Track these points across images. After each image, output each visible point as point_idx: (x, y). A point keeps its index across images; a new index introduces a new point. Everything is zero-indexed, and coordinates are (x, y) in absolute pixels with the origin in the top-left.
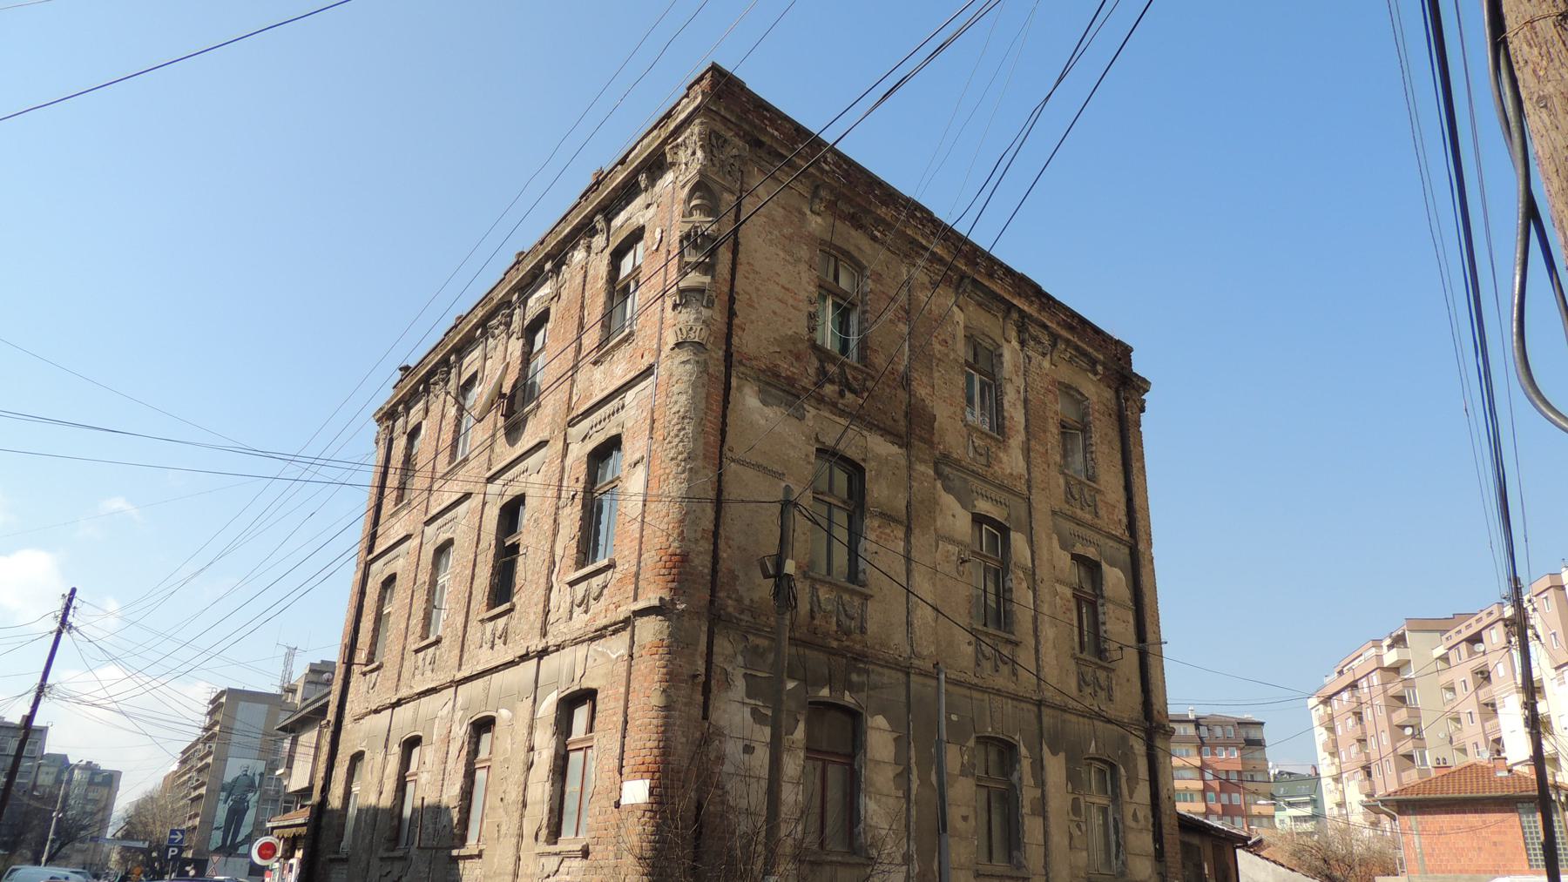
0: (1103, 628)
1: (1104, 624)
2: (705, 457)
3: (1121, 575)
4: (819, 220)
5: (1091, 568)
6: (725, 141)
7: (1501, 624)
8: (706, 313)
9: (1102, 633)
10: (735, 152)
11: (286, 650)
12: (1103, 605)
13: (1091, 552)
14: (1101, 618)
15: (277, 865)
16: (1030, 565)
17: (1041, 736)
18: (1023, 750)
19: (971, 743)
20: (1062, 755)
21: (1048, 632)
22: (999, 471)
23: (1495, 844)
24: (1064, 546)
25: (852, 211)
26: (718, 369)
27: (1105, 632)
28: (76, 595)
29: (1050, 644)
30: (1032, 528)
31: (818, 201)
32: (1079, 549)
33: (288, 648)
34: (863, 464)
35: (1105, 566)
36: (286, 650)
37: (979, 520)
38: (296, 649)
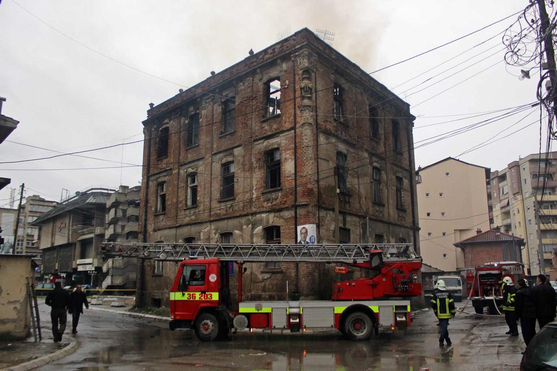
0: (403, 199)
2: (314, 159)
3: (408, 181)
4: (333, 76)
5: (399, 180)
7: (496, 179)
8: (311, 113)
10: (314, 58)
11: (11, 190)
13: (400, 175)
15: (399, 286)
16: (386, 180)
18: (385, 237)
19: (374, 236)
20: (394, 239)
21: (391, 201)
22: (378, 152)
23: (494, 256)
26: (315, 131)
28: (25, 186)
29: (391, 206)
32: (397, 175)
33: (12, 189)
34: (347, 155)
35: (404, 179)
36: (11, 190)
37: (374, 168)
38: (15, 189)
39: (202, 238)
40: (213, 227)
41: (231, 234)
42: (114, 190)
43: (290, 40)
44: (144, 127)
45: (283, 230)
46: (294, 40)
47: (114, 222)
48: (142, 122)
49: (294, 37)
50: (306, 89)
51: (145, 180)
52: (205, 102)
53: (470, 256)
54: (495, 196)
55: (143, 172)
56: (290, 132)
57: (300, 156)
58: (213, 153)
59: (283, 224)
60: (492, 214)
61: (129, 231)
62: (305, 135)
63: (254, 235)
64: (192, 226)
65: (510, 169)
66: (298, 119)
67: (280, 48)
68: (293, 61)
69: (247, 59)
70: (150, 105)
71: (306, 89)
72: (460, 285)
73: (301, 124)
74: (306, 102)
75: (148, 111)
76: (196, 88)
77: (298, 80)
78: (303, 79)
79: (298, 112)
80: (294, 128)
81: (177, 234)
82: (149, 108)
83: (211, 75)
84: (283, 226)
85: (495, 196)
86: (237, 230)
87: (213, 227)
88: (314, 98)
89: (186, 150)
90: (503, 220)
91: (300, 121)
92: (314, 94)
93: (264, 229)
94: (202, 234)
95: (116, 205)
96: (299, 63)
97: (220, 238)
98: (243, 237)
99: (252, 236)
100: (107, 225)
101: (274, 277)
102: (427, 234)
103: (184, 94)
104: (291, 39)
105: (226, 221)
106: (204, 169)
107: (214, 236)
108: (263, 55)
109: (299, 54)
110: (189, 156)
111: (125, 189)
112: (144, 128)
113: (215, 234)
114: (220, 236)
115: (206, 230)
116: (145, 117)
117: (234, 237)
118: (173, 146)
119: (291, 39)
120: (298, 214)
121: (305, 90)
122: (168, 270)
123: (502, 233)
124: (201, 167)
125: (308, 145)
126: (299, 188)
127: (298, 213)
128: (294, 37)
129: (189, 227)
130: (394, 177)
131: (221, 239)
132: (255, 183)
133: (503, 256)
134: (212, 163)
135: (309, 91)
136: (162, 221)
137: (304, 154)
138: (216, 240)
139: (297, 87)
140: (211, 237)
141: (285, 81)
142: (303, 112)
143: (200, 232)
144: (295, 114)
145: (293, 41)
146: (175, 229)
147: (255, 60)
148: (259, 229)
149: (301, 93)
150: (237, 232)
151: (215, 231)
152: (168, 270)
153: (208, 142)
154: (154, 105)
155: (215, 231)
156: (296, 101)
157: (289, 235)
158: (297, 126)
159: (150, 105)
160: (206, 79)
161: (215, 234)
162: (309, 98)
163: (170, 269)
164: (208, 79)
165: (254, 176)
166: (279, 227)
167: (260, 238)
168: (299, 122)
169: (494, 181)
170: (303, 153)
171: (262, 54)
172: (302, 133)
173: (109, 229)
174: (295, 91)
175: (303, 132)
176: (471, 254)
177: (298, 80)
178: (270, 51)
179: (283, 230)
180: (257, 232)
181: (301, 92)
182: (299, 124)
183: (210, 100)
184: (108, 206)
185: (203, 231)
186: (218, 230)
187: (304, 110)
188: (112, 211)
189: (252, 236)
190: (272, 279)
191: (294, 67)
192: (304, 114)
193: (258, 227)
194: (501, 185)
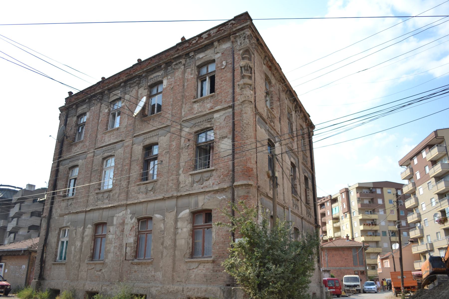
1: (309, 196)
6: (252, 37)
9: (308, 198)
12: (308, 190)
14: (308, 194)
17: (303, 228)
23: (346, 259)
24: (303, 173)
31: (265, 60)
39: (115, 222)
40: (129, 211)
41: (151, 218)
42: (21, 188)
43: (228, 24)
45: (216, 213)
46: (233, 24)
47: (18, 216)
49: (233, 22)
51: (56, 164)
53: (326, 258)
56: (226, 111)
57: (239, 134)
58: (135, 135)
59: (215, 207)
61: (31, 225)
62: (245, 113)
65: (341, 193)
67: (216, 32)
68: (233, 42)
72: (359, 282)
73: (241, 101)
74: (247, 80)
75: (66, 99)
77: (237, 59)
78: (243, 58)
79: (237, 90)
80: (233, 107)
82: (67, 96)
83: (137, 62)
84: (215, 209)
85: (329, 214)
86: (158, 214)
89: (104, 133)
90: (334, 233)
91: (240, 99)
92: (253, 74)
94: (115, 219)
95: (21, 201)
97: (136, 223)
98: (165, 221)
100: (11, 219)
101: (203, 267)
102: (57, 287)
103: (106, 81)
105: (145, 205)
106: (123, 152)
107: (130, 220)
108: (197, 40)
109: (240, 35)
110: (107, 139)
111: (31, 187)
112: (60, 114)
113: (131, 218)
114: (136, 221)
115: (121, 214)
117: (154, 221)
118: (90, 130)
119: (230, 23)
120: (235, 196)
121: (246, 68)
122: (72, 257)
123: (350, 240)
124: (119, 150)
127: (236, 194)
128: (233, 22)
129: (101, 211)
130: (303, 175)
131: (137, 224)
135: (250, 70)
137: (244, 132)
138: (132, 226)
139: (237, 66)
140: (126, 222)
141: (222, 62)
142: (243, 90)
143: (113, 217)
144: (234, 93)
146: (84, 214)
148: (185, 213)
149: (242, 72)
150: (158, 216)
151: (131, 215)
152: (72, 257)
153: (130, 125)
154: (73, 93)
155: (131, 215)
158: (237, 103)
159: (69, 93)
160: (131, 65)
161: (131, 218)
163: (75, 256)
164: (134, 66)
166: (211, 210)
167: (186, 223)
168: (239, 100)
170: (243, 131)
171: (195, 40)
172: (242, 111)
173: (12, 222)
174: (234, 70)
175: (243, 109)
176: (327, 257)
177: (237, 59)
178: (205, 36)
179: (216, 213)
180: (182, 216)
182: (238, 101)
185: (117, 215)
187: (245, 88)
189: (176, 221)
190: (200, 270)
192: (245, 92)
193: (184, 210)
194: (334, 205)
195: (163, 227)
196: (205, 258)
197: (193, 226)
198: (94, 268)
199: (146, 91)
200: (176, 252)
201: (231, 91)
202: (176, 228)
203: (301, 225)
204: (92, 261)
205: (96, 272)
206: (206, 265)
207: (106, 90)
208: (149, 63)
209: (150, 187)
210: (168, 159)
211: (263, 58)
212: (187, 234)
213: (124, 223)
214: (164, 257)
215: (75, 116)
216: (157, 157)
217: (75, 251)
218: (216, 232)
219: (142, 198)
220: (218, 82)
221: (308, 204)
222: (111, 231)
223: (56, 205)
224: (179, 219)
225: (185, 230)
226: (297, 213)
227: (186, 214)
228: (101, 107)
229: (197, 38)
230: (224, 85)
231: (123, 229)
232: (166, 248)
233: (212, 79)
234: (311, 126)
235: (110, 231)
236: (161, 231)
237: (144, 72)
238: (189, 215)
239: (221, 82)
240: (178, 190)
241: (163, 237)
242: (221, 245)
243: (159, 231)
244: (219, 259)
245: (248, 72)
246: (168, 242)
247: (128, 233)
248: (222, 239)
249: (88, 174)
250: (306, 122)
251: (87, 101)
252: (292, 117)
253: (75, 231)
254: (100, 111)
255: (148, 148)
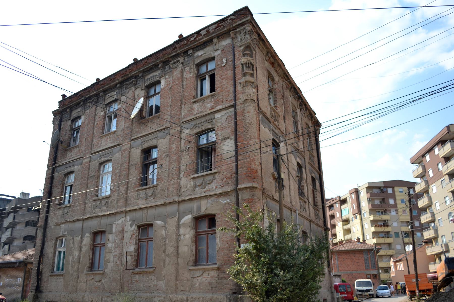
1: (316, 197)
6: (253, 33)
9: (316, 200)
12: (316, 192)
14: (315, 196)
23: (357, 263)
25: (273, 61)
27: (317, 200)
30: (306, 167)
39: (114, 231)
42: (15, 197)
43: (227, 20)
44: (54, 117)
46: (232, 19)
48: (53, 112)
50: (249, 65)
52: (125, 88)
54: (338, 216)
55: (50, 152)
56: (228, 111)
57: (242, 135)
59: (219, 212)
60: (335, 230)
61: (26, 235)
63: (181, 225)
64: (103, 218)
65: (350, 194)
66: (239, 96)
67: (215, 28)
69: (176, 42)
70: (62, 96)
71: (249, 65)
76: (115, 76)
77: (238, 56)
79: (239, 88)
80: (234, 106)
81: (84, 227)
82: (61, 99)
84: (219, 214)
85: (338, 216)
87: (128, 218)
88: (255, 75)
90: (344, 235)
91: (241, 97)
92: (255, 72)
93: (194, 218)
94: (114, 226)
95: (15, 210)
96: (239, 39)
98: (166, 228)
99: (178, 227)
100: (5, 229)
104: (229, 19)
106: (120, 156)
107: (130, 228)
108: (195, 37)
110: (103, 143)
111: (25, 195)
112: (53, 118)
113: (131, 226)
114: (136, 228)
115: (120, 221)
116: (56, 107)
119: (229, 19)
120: (240, 199)
122: (70, 268)
124: (117, 154)
125: (251, 122)
126: (240, 170)
127: (240, 197)
132: (183, 167)
133: (365, 262)
134: (130, 149)
135: (251, 67)
136: (67, 213)
137: (247, 132)
138: (132, 233)
139: (238, 63)
142: (244, 88)
143: (112, 225)
144: (235, 91)
145: (231, 21)
146: (81, 222)
147: (186, 43)
148: (188, 218)
149: (243, 70)
151: (131, 222)
152: (70, 268)
153: (127, 127)
155: (131, 222)
156: (236, 78)
157: (228, 224)
158: (238, 102)
159: (62, 96)
160: (127, 65)
161: (131, 226)
162: (252, 75)
163: (73, 267)
164: (130, 65)
165: (183, 160)
166: (214, 215)
167: (189, 229)
168: (241, 99)
169: (337, 204)
170: (246, 131)
171: (193, 37)
173: (6, 233)
175: (246, 108)
176: (338, 260)
177: (238, 56)
178: (203, 33)
180: (184, 221)
181: (243, 67)
183: (131, 85)
184: (7, 211)
185: (116, 222)
186: (134, 221)
188: (11, 216)
189: (178, 227)
191: (233, 44)
193: (186, 216)
194: (343, 207)
195: (164, 234)
196: (209, 265)
197: (196, 232)
198: (93, 279)
199: (144, 91)
200: (179, 260)
201: (232, 89)
202: (178, 235)
203: (309, 228)
204: (91, 271)
205: (95, 282)
206: (211, 272)
207: (101, 92)
208: (146, 62)
209: (150, 192)
210: (168, 162)
211: (265, 55)
212: (190, 241)
213: (124, 230)
214: (166, 265)
215: (69, 120)
216: (157, 161)
217: (73, 261)
218: (221, 238)
219: (142, 204)
220: (218, 80)
221: (316, 206)
222: (110, 239)
223: (51, 214)
224: (181, 225)
225: (187, 236)
226: (305, 215)
227: (188, 219)
228: (96, 109)
229: (196, 35)
230: (224, 83)
231: (122, 237)
232: (168, 255)
233: (213, 78)
234: (317, 124)
235: (109, 240)
236: (162, 238)
237: (140, 72)
238: (192, 221)
239: (221, 81)
240: (179, 195)
241: (165, 245)
242: (225, 251)
243: (161, 238)
244: (225, 266)
245: (249, 69)
246: (170, 250)
247: (129, 241)
248: (227, 245)
249: (84, 180)
250: (312, 120)
251: (81, 103)
252: (297, 115)
253: (72, 240)
254: (95, 114)
255: (147, 152)
